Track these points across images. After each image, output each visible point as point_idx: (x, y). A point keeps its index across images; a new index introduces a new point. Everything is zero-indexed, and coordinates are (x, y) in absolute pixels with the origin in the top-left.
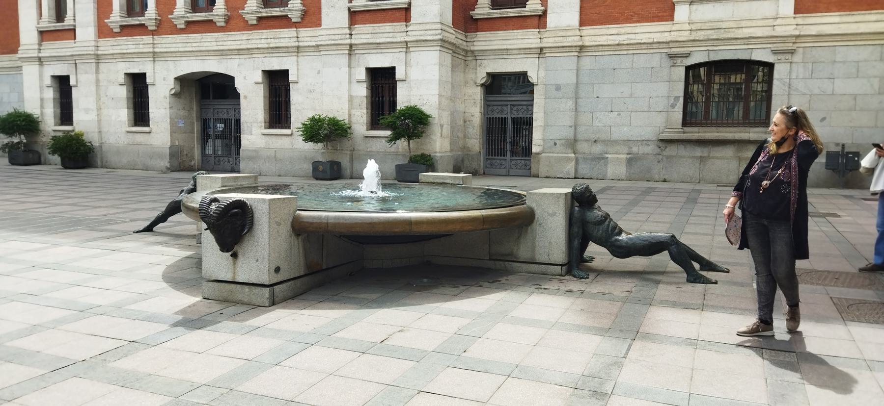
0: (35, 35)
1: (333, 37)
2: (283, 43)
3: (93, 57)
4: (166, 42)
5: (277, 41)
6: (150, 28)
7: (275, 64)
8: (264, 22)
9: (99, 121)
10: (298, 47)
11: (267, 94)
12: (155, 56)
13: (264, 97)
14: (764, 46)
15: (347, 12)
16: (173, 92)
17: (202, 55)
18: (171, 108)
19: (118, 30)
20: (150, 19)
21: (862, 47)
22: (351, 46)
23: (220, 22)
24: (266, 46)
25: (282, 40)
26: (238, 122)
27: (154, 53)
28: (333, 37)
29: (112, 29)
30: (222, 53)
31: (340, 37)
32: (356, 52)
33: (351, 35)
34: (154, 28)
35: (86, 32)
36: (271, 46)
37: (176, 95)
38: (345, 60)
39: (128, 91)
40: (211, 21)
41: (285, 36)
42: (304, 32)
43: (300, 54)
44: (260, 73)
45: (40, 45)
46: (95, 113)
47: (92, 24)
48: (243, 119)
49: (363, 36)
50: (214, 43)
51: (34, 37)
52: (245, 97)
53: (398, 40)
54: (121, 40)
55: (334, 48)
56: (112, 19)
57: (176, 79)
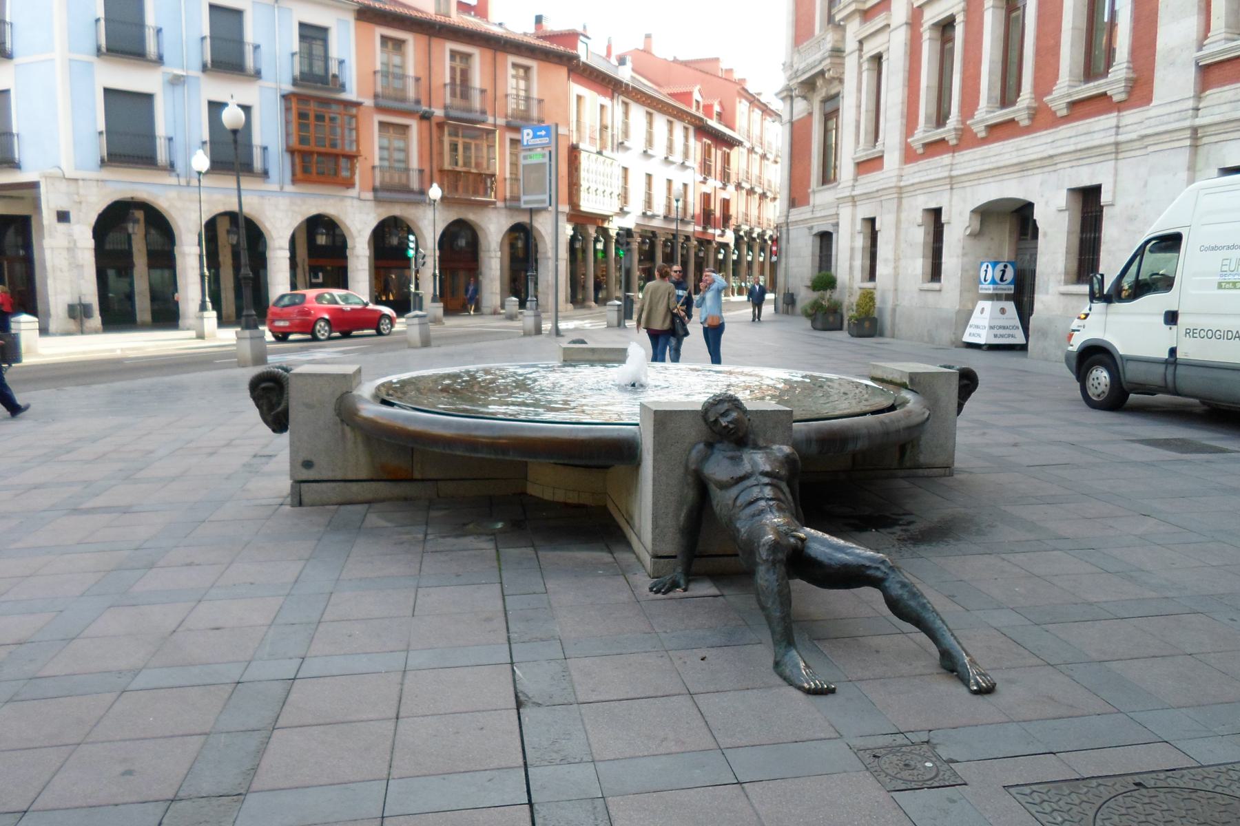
0: (1191, 74)
1: (1165, 119)
2: (1097, 140)
3: (894, 190)
4: (970, 160)
5: (1088, 137)
6: (1115, 99)
7: (1085, 179)
8: (1216, 72)
9: (896, 276)
10: (1117, 144)
11: (1078, 228)
12: (952, 182)
13: (1069, 233)
14: (1177, 144)
15: (1193, 69)
16: (968, 232)
17: (990, 173)
18: (964, 255)
19: (1064, 112)
20: (1118, 81)
21: (1161, 154)
22: (1195, 130)
23: (1025, 122)
24: (1072, 148)
25: (1096, 136)
26: (1034, 271)
27: (951, 177)
28: (1165, 119)
29: (1054, 113)
30: (1023, 168)
31: (1177, 116)
32: (1205, 140)
33: (1197, 109)
34: (1123, 97)
35: (892, 159)
36: (1080, 146)
37: (975, 235)
38: (1183, 157)
39: (926, 234)
40: (1104, 95)
41: (1100, 128)
42: (1131, 117)
43: (1121, 156)
44: (1065, 192)
45: (1198, 97)
46: (892, 265)
47: (898, 146)
48: (1039, 269)
49: (1216, 110)
50: (1014, 154)
51: (1188, 78)
52: (1045, 235)
53: (941, 176)
54: (996, 147)
55: (1166, 137)
56: (1056, 94)
57: (974, 212)
